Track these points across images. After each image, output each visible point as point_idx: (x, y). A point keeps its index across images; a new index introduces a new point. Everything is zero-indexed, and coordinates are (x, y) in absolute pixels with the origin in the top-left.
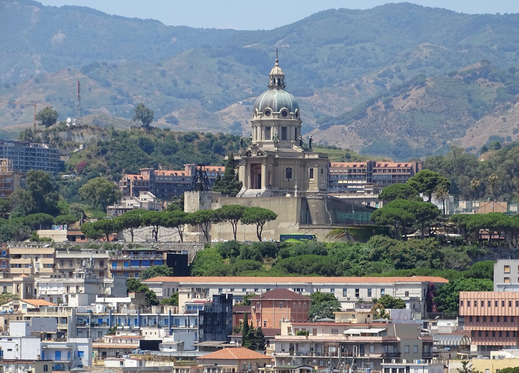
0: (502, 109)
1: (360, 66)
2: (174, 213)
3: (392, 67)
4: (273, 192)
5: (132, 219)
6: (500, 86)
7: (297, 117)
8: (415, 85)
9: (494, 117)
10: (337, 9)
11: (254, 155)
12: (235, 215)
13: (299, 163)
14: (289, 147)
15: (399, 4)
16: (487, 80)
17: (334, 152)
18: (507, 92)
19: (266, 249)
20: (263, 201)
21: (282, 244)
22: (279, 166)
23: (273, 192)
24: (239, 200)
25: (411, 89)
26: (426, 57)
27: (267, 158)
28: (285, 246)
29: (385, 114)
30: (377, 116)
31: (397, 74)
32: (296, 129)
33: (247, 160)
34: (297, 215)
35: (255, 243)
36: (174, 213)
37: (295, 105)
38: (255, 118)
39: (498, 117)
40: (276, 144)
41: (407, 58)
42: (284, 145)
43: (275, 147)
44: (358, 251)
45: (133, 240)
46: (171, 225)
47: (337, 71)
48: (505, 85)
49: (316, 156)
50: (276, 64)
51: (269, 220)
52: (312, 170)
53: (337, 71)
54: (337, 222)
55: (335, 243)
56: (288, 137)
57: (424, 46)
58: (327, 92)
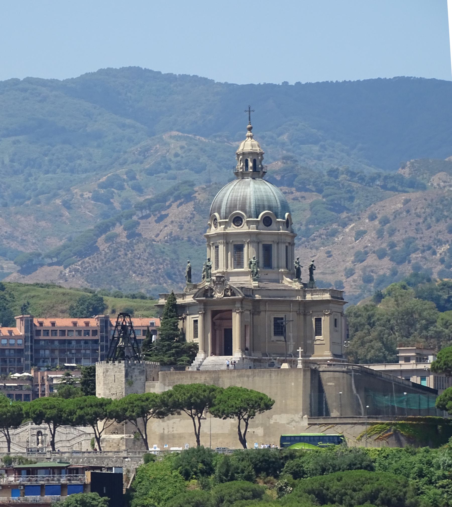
0: (324, 237)
1: (63, 171)
2: (85, 401)
3: (122, 172)
4: (251, 360)
5: (9, 411)
6: (315, 198)
7: (287, 227)
8: (177, 198)
9: (311, 248)
10: (22, 79)
11: (218, 295)
12: (200, 402)
13: (296, 308)
14: (277, 281)
15: (123, 69)
16: (294, 189)
17: (142, 304)
18: (326, 208)
19: (261, 462)
20: (240, 376)
21: (286, 452)
22: (262, 313)
23: (251, 360)
24: (197, 376)
25: (170, 206)
26: (176, 155)
27: (242, 300)
28: (292, 456)
29: (130, 246)
30: (116, 250)
31: (130, 183)
32: (287, 247)
33: (205, 304)
34: (304, 401)
35: (237, 452)
36: (85, 401)
37: (285, 207)
38: (213, 231)
39: (317, 249)
40: (255, 275)
41: (144, 156)
42: (267, 277)
43: (254, 280)
44: (429, 463)
45: (9, 451)
46: (82, 421)
47: (27, 180)
48: (323, 197)
49: (327, 296)
50: (249, 133)
51: (261, 410)
52: (318, 321)
53: (27, 180)
54: (375, 412)
55: (382, 451)
56: (274, 263)
57: (171, 137)
58: (16, 213)
